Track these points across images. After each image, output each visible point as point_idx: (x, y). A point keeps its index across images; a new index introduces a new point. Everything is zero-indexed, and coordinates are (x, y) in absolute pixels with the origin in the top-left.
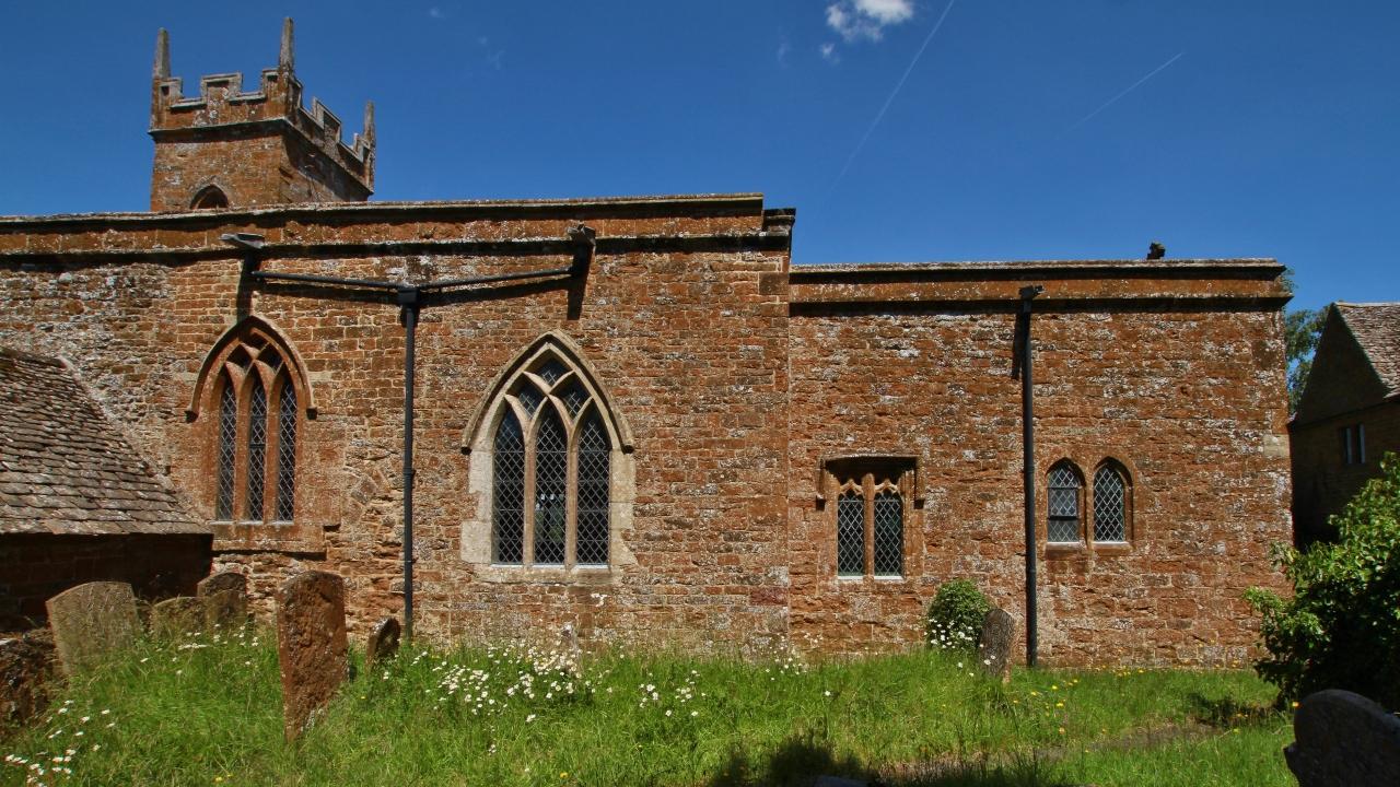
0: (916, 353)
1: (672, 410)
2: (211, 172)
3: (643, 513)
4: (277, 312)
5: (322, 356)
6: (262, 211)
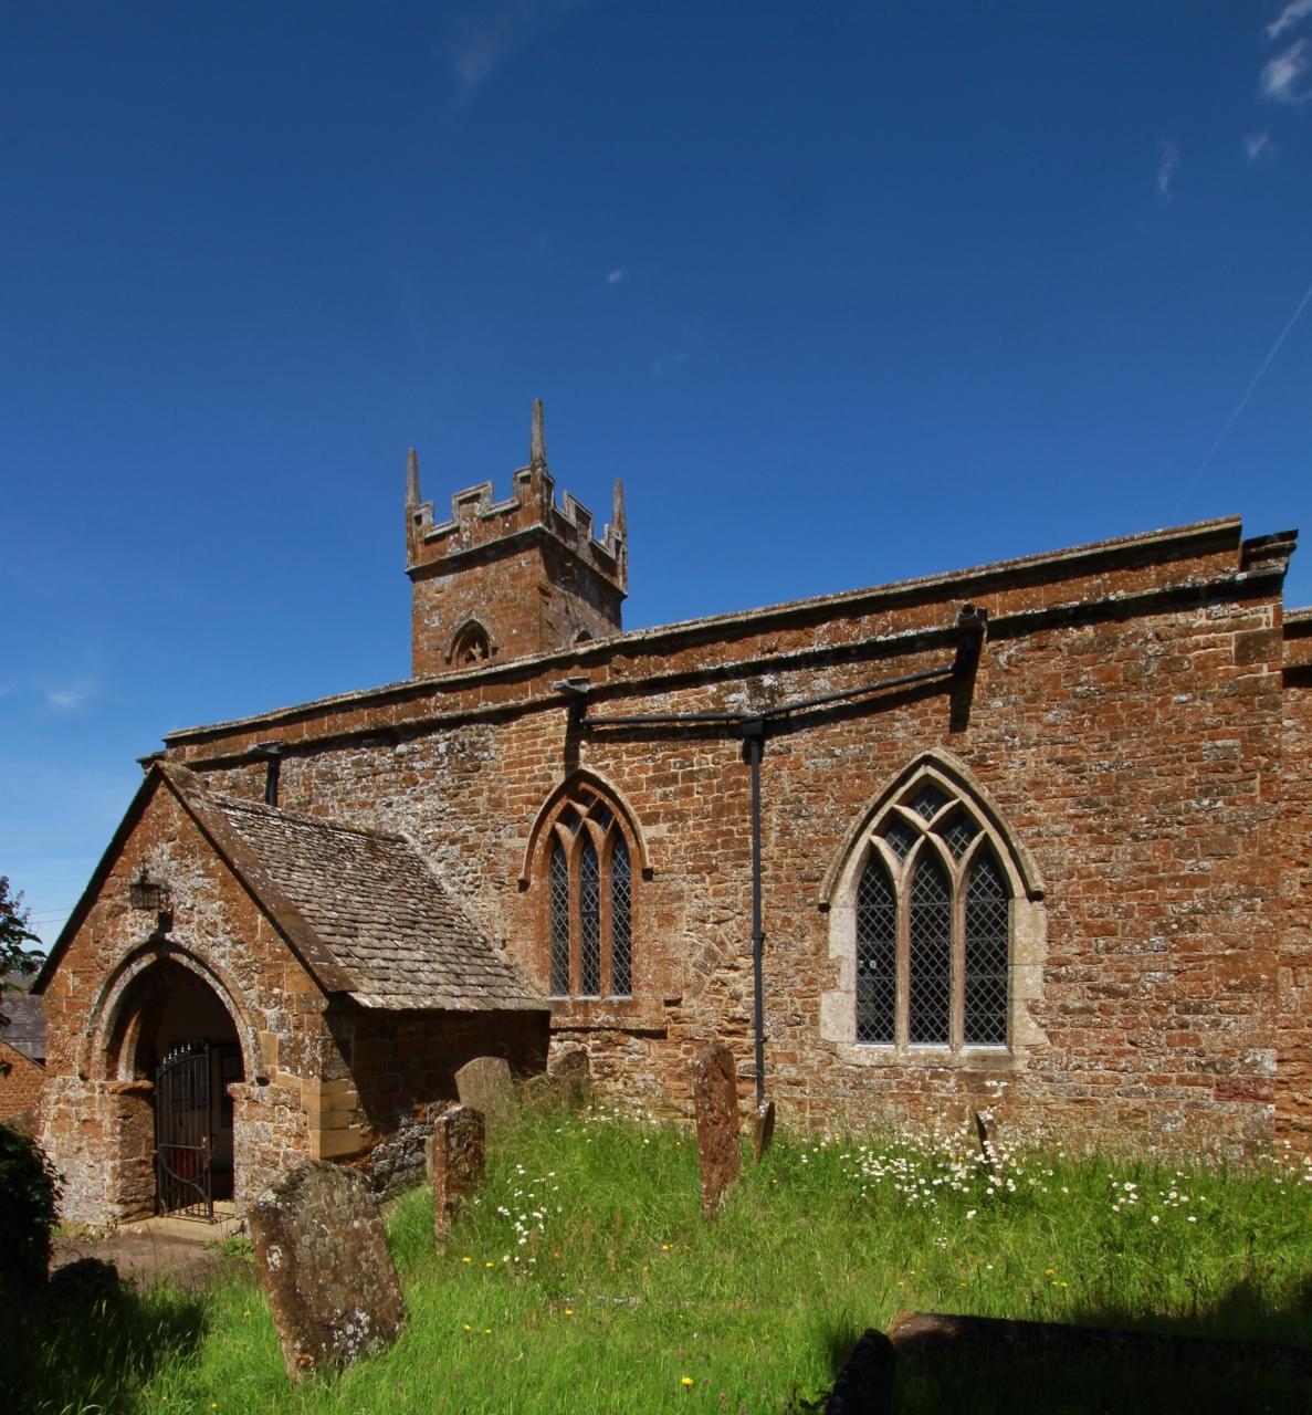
1: (1100, 840)
3: (1057, 978)
4: (606, 762)
5: (656, 807)
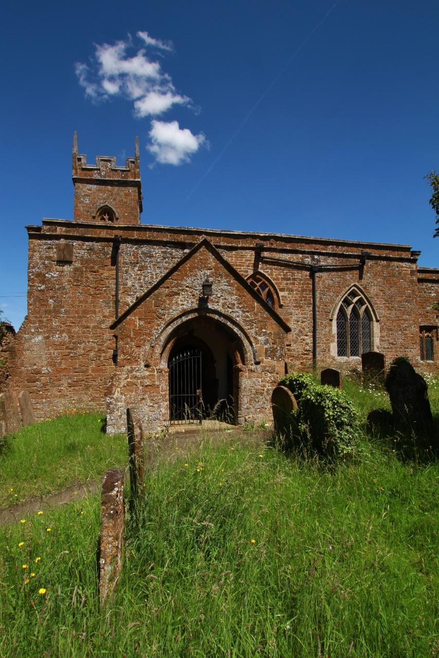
0: (435, 295)
1: (389, 310)
2: (104, 199)
3: (382, 341)
6: (264, 235)
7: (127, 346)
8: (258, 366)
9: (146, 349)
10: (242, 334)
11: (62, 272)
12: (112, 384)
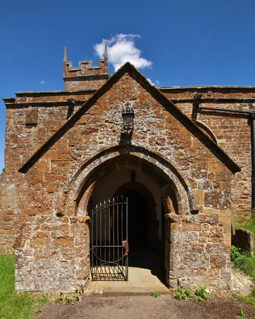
4: (206, 120)
5: (222, 134)
7: (39, 192)
8: (195, 216)
9: (59, 195)
10: (174, 175)
11: (30, 133)
12: (21, 235)
